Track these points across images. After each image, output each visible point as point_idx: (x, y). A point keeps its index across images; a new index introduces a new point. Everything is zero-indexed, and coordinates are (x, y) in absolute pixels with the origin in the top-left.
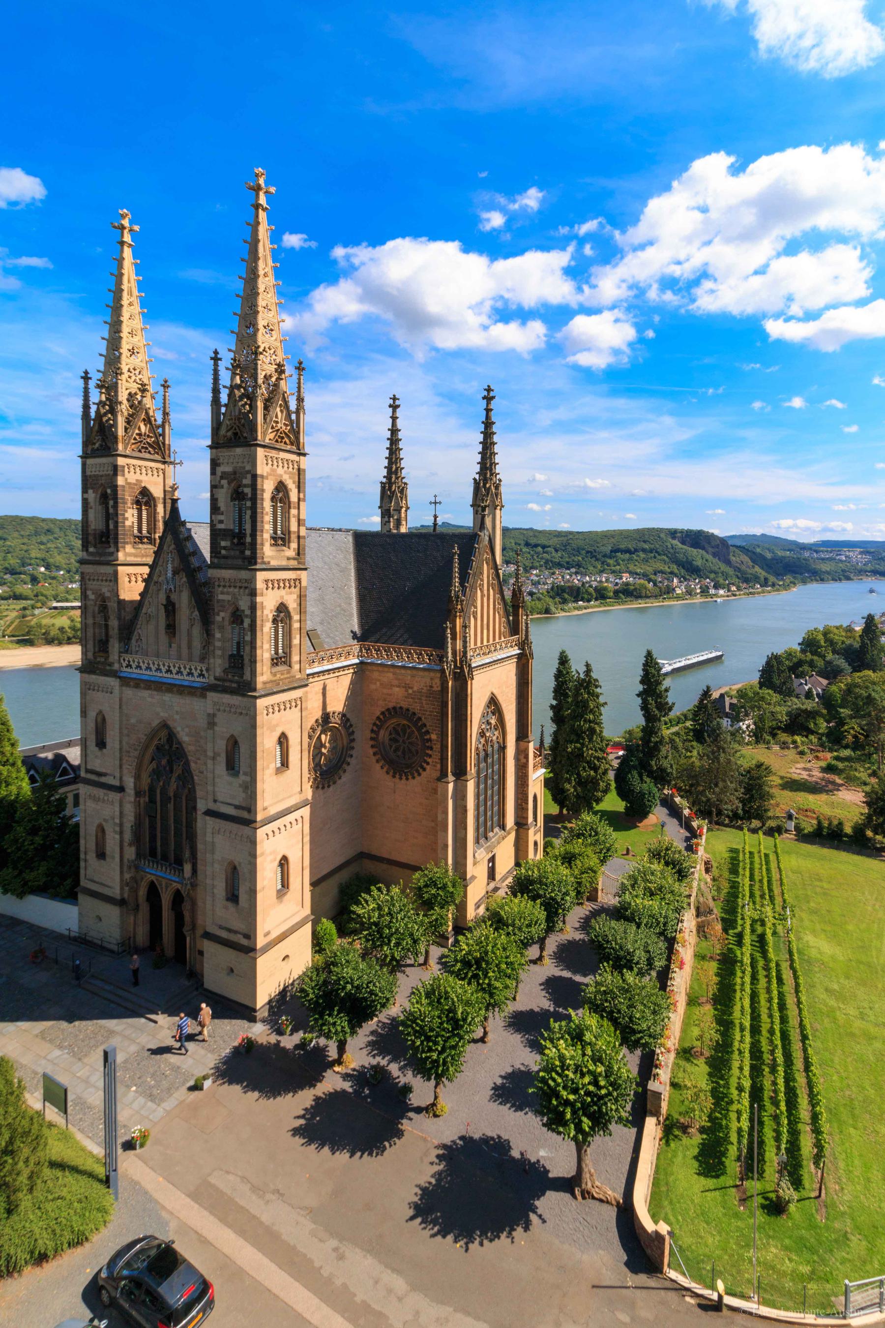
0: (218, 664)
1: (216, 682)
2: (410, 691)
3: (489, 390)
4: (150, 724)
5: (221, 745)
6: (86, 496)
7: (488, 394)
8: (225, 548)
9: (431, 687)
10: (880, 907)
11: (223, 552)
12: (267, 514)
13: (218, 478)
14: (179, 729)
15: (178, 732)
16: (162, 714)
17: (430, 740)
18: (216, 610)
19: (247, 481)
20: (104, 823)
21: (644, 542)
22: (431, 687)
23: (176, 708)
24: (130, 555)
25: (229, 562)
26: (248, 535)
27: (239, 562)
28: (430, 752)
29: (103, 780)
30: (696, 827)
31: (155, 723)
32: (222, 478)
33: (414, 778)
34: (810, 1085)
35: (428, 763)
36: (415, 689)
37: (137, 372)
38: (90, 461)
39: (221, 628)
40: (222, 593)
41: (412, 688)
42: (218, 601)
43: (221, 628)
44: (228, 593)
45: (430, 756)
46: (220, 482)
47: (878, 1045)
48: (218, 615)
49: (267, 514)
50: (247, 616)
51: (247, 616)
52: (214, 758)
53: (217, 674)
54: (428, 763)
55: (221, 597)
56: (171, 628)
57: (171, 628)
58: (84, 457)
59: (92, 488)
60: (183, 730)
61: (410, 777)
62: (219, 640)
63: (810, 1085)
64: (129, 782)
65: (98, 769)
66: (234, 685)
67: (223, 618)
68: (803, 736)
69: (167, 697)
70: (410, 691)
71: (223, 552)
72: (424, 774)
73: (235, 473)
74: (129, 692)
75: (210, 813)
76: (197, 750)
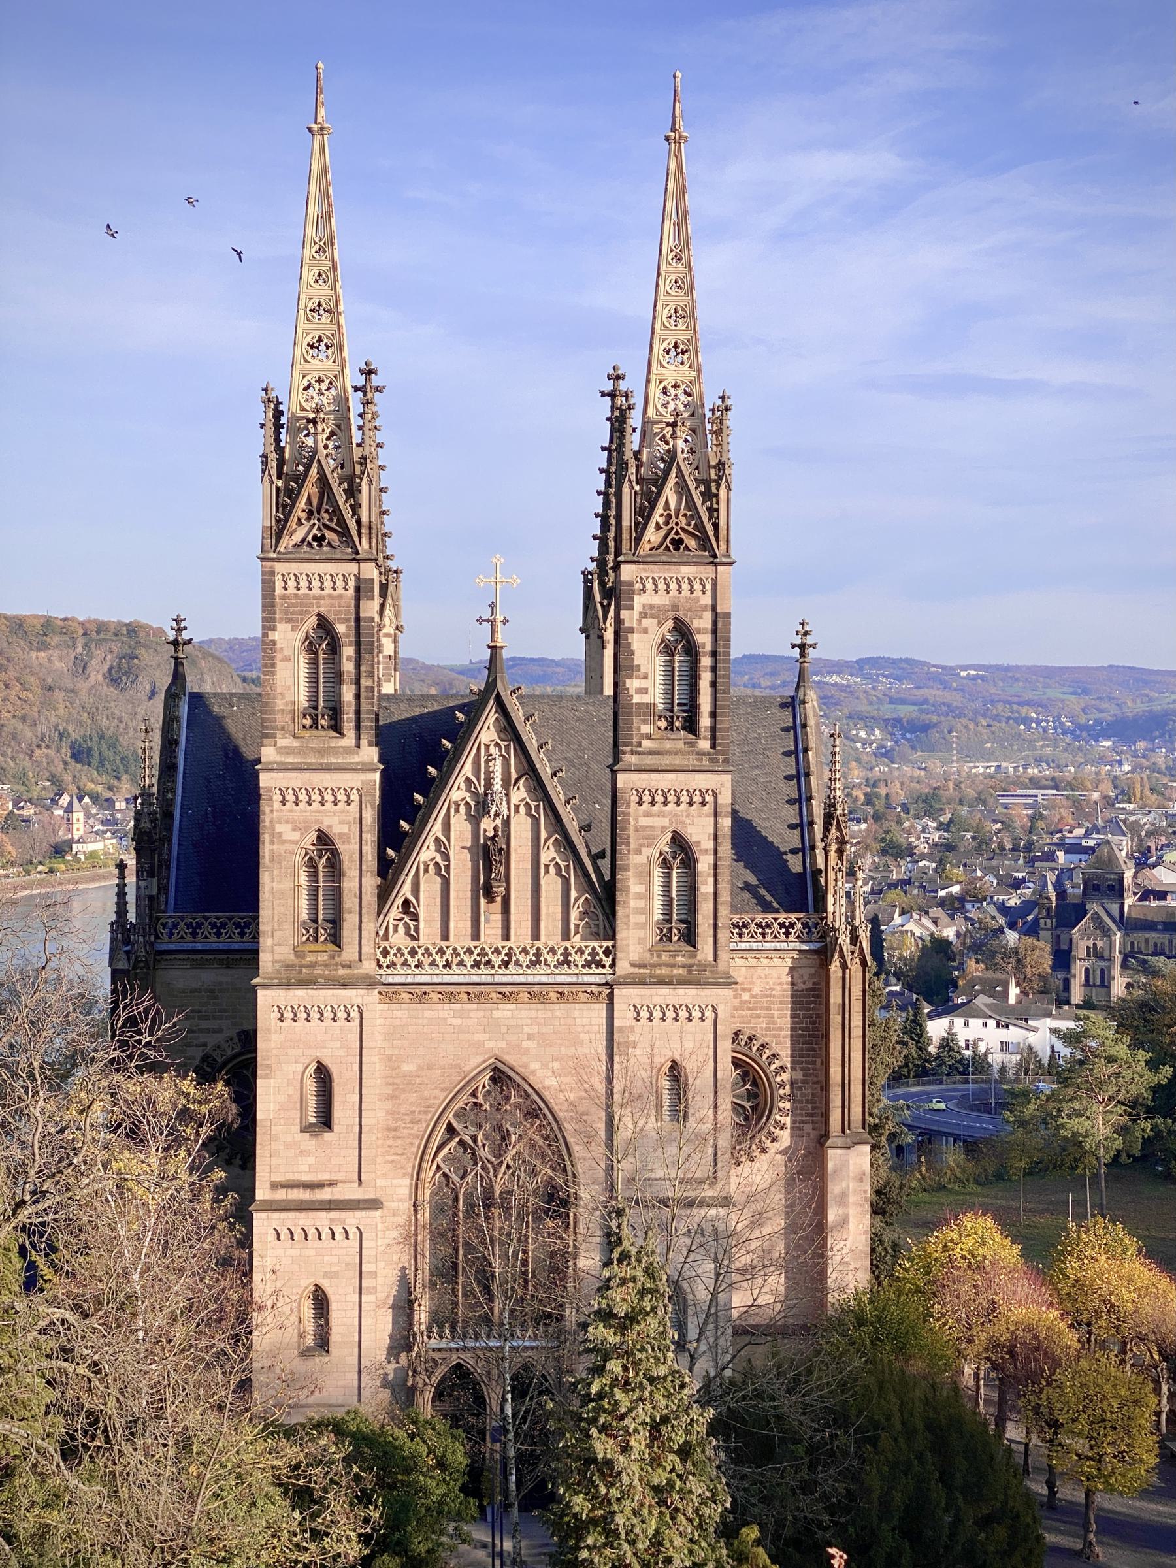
1: (636, 970)
8: (649, 737)
11: (646, 744)
12: (758, 1542)
14: (534, 1066)
16: (490, 1044)
18: (633, 846)
21: (754, 686)
23: (526, 1030)
24: (288, 751)
27: (692, 761)
29: (326, 1194)
34: (530, 1086)
36: (756, 990)
37: (324, 386)
41: (750, 990)
47: (2, 948)
49: (348, 659)
55: (644, 821)
63: (530, 1086)
65: (306, 1178)
66: (681, 971)
69: (505, 1011)
71: (646, 744)
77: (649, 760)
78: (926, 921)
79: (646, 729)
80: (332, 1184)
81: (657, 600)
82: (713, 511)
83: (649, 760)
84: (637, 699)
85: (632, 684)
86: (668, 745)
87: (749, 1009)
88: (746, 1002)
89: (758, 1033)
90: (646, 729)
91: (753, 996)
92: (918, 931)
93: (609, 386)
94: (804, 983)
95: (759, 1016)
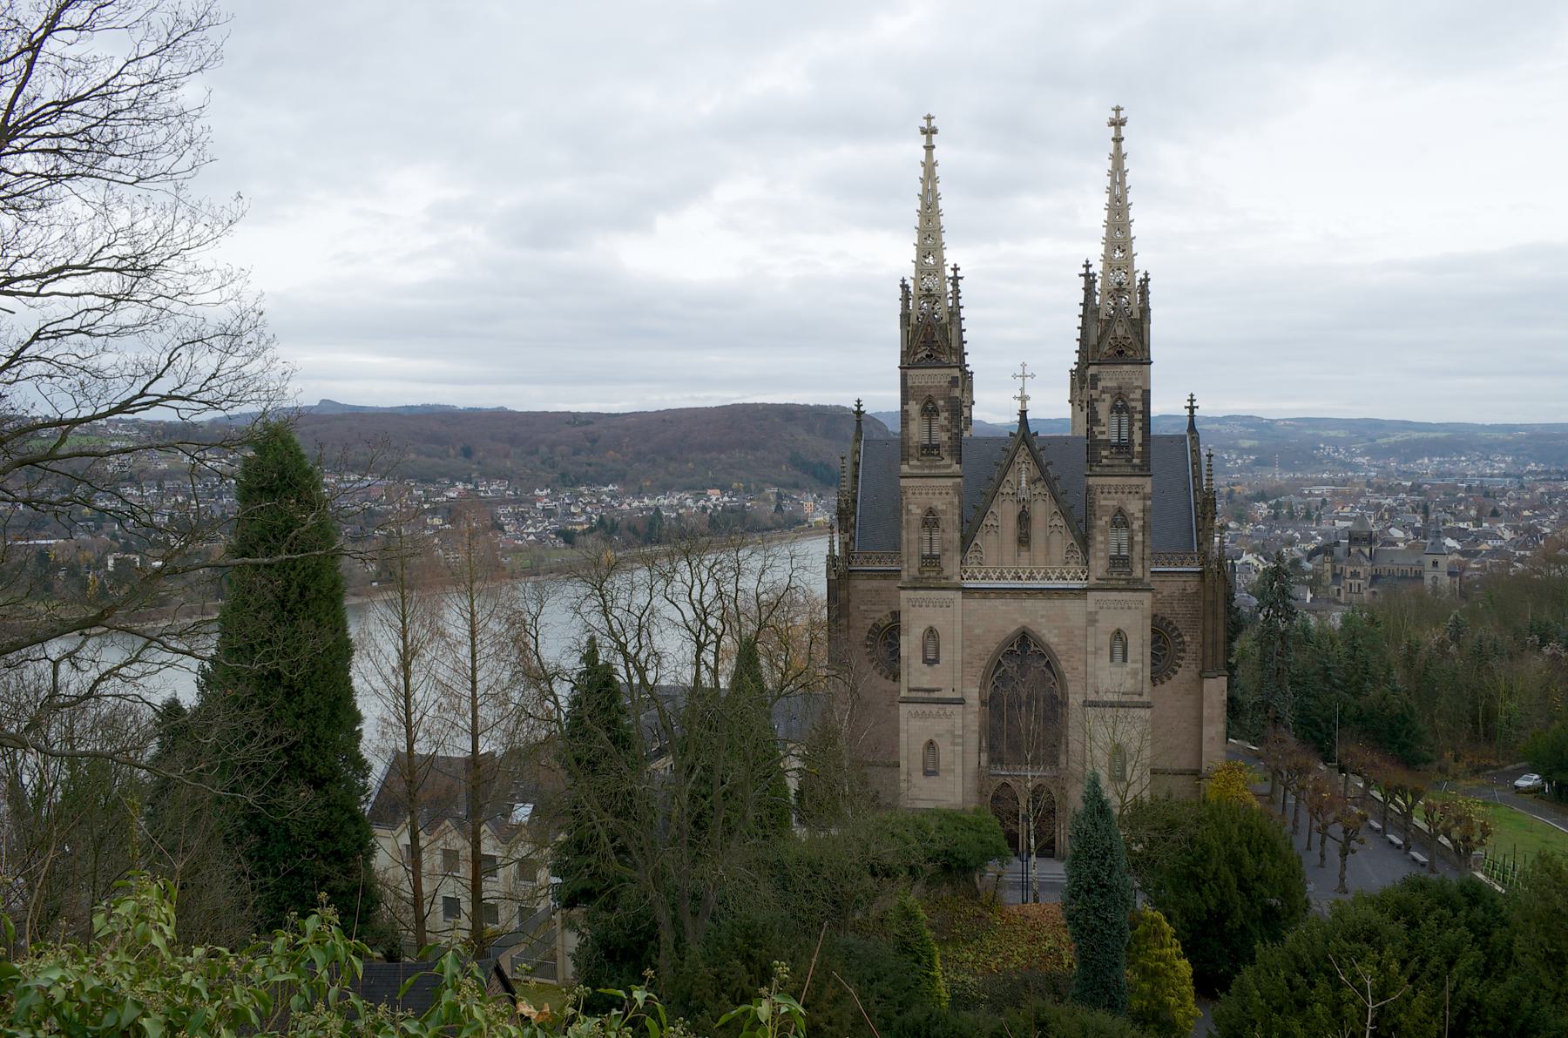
0: (1099, 566)
2: (1159, 596)
5: (1105, 640)
6: (906, 407)
7: (1087, 270)
8: (1106, 457)
9: (1185, 590)
14: (1044, 631)
15: (1044, 635)
17: (1183, 642)
19: (1138, 394)
22: (1185, 590)
25: (1116, 470)
27: (1129, 470)
28: (1182, 654)
29: (936, 695)
32: (1103, 392)
33: (1163, 683)
35: (1180, 666)
36: (1165, 593)
38: (910, 372)
40: (1105, 499)
42: (1100, 507)
44: (1113, 499)
45: (1182, 658)
52: (1095, 653)
53: (1099, 575)
54: (1180, 666)
55: (1103, 503)
56: (1024, 540)
57: (1024, 540)
58: (905, 367)
59: (915, 400)
60: (1049, 632)
61: (1158, 683)
62: (1102, 542)
64: (973, 694)
70: (1159, 596)
71: (1104, 461)
72: (1175, 677)
73: (1120, 388)
74: (973, 604)
75: (1088, 704)
77: (1107, 470)
79: (1104, 453)
80: (939, 690)
83: (1107, 470)
86: (1116, 462)
89: (1166, 616)
90: (1104, 453)
92: (1256, 563)
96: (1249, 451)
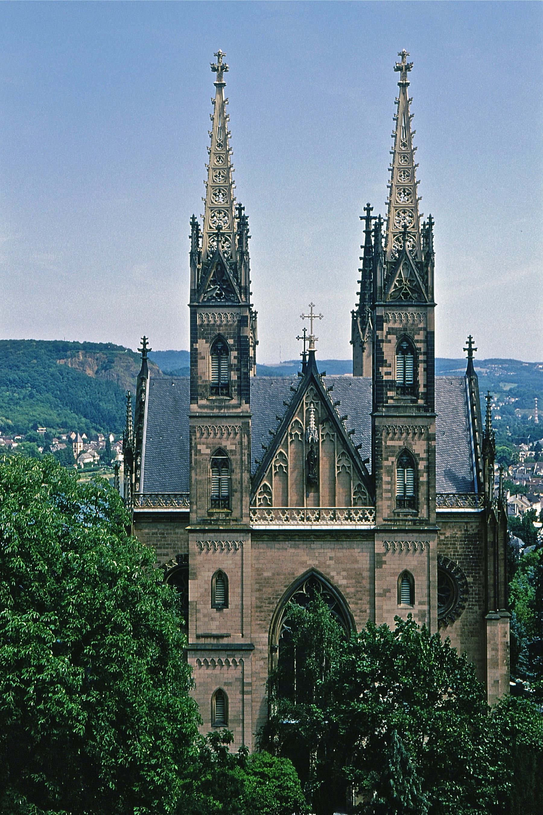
3: (144, 339)
4: (293, 574)
10: (34, 646)
13: (385, 333)
14: (333, 574)
15: (333, 577)
19: (420, 336)
20: (225, 688)
26: (422, 386)
28: (465, 596)
30: (348, 602)
31: (302, 571)
39: (390, 472)
42: (387, 447)
43: (390, 472)
44: (399, 439)
46: (386, 337)
48: (387, 459)
50: (422, 459)
51: (422, 459)
55: (389, 443)
60: (338, 574)
65: (214, 632)
67: (393, 462)
68: (470, 534)
76: (357, 591)
78: (525, 499)
79: (390, 394)
81: (397, 326)
82: (425, 282)
84: (385, 378)
85: (383, 370)
87: (444, 544)
88: (442, 540)
90: (390, 394)
91: (446, 537)
92: (520, 503)
93: (365, 214)
94: (473, 530)
95: (449, 548)
96: (511, 393)
